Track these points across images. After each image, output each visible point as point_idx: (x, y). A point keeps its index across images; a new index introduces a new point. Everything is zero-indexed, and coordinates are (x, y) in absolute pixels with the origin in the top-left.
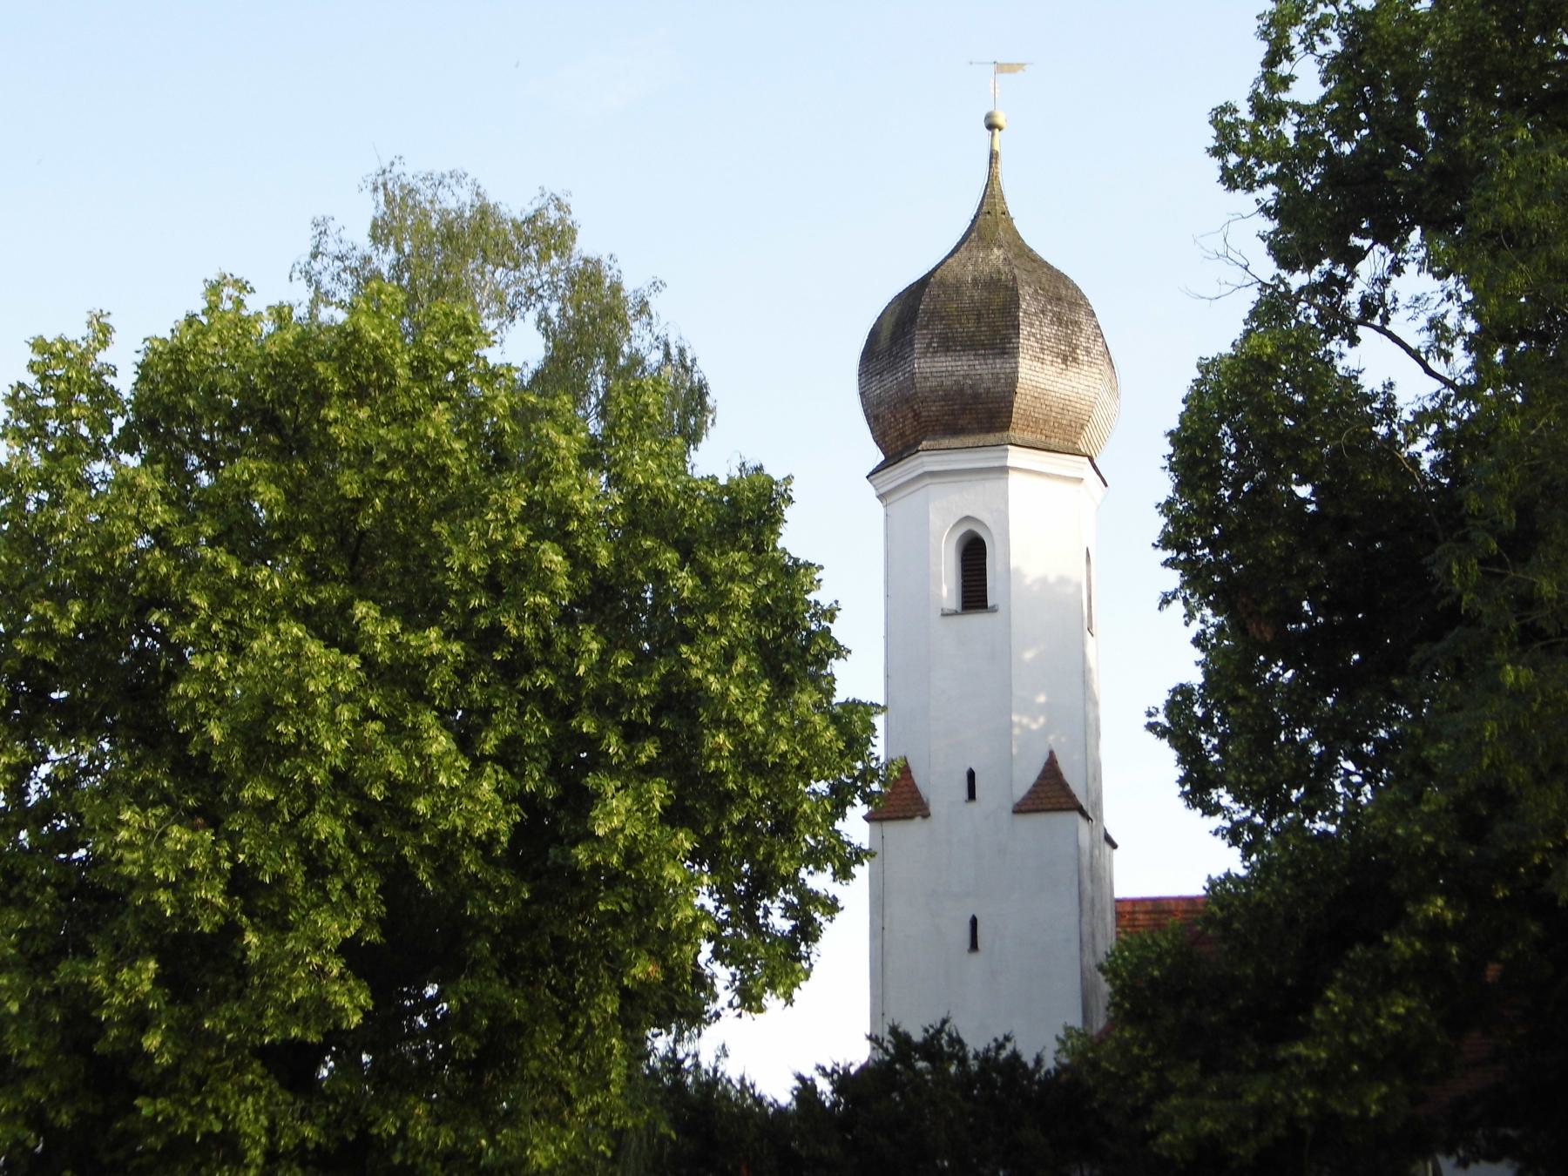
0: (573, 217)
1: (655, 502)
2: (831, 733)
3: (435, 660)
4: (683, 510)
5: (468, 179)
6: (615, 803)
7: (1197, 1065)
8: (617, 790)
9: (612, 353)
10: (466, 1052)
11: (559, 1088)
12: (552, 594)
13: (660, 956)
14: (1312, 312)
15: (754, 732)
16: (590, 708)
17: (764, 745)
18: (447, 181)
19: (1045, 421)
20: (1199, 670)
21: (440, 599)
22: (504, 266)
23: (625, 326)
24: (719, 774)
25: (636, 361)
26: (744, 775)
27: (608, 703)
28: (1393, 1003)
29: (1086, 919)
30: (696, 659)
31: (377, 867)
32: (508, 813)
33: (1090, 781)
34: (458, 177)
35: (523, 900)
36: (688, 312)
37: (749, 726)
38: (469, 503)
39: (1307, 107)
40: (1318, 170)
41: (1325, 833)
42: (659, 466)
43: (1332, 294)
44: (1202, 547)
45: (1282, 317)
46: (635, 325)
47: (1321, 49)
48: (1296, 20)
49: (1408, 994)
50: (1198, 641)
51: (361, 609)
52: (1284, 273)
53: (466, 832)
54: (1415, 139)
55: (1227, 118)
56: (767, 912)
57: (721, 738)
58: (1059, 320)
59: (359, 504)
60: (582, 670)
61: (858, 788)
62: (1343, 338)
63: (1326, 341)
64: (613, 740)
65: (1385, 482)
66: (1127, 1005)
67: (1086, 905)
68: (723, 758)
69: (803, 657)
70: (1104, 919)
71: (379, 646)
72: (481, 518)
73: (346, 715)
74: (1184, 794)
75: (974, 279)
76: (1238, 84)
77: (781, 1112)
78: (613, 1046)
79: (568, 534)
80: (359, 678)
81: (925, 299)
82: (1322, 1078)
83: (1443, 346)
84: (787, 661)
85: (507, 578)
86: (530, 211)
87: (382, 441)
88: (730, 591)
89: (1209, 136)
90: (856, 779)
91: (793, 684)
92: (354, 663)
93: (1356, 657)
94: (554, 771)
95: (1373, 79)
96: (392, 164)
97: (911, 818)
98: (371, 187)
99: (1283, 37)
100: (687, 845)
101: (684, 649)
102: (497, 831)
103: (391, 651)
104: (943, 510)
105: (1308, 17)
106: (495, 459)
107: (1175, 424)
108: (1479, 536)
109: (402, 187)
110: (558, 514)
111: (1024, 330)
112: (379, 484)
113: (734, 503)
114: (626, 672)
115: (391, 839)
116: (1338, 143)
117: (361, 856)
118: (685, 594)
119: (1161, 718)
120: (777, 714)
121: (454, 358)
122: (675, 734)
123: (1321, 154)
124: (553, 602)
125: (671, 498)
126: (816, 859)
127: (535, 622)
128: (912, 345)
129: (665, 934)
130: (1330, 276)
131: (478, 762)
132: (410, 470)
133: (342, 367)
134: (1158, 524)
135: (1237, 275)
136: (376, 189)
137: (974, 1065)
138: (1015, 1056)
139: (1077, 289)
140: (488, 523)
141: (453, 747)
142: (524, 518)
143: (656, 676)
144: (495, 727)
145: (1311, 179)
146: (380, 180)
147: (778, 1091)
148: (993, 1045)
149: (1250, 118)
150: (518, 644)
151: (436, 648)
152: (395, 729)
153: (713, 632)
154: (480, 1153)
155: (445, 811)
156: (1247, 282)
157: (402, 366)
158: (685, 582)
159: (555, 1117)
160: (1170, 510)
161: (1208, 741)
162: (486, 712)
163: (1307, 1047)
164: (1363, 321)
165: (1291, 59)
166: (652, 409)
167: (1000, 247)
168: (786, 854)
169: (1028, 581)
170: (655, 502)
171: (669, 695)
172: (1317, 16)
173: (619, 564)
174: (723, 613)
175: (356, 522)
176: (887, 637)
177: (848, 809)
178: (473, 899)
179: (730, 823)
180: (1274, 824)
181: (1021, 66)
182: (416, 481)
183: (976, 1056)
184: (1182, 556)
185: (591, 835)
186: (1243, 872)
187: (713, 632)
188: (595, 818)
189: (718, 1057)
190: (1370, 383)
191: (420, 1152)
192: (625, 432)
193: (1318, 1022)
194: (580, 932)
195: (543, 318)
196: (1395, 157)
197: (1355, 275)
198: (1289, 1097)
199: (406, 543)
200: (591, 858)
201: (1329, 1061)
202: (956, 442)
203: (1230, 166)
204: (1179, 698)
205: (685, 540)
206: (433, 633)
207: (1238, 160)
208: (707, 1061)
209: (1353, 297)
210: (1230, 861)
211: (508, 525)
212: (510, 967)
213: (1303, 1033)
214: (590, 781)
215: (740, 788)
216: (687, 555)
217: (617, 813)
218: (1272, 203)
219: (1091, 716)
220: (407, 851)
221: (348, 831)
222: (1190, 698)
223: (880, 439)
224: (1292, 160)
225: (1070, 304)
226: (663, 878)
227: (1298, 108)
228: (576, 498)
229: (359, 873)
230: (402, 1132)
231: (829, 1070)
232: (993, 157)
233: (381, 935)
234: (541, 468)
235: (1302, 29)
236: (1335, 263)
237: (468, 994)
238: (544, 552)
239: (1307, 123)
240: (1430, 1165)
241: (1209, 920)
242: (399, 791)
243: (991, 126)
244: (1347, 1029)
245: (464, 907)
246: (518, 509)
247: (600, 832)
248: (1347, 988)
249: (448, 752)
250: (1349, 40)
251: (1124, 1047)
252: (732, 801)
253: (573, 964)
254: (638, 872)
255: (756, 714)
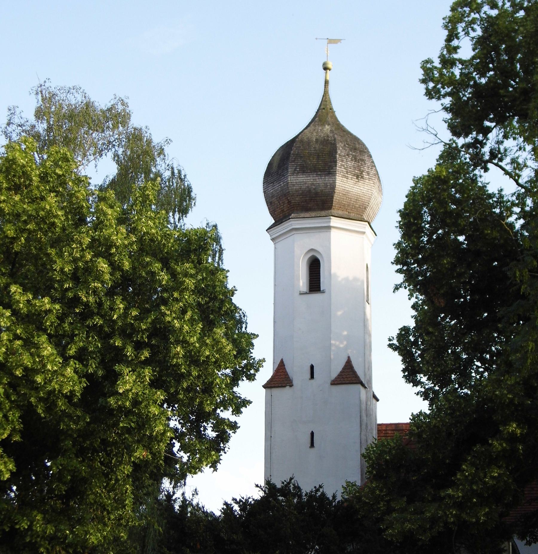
0: (129, 109)
1: (152, 240)
2: (230, 347)
3: (50, 311)
4: (164, 244)
5: (81, 90)
6: (128, 378)
7: (405, 499)
8: (130, 372)
9: (148, 172)
10: (61, 491)
11: (104, 508)
12: (103, 282)
13: (148, 448)
14: (468, 156)
15: (195, 346)
16: (120, 335)
17: (199, 352)
18: (72, 91)
19: (349, 205)
20: (413, 320)
21: (51, 284)
22: (97, 131)
23: (154, 160)
24: (178, 365)
25: (158, 174)
26: (189, 366)
27: (128, 332)
28: (492, 472)
29: (363, 433)
30: (168, 312)
31: (18, 407)
32: (80, 383)
33: (367, 370)
34: (76, 89)
35: (87, 422)
36: (182, 154)
37: (192, 344)
38: (61, 241)
39: (465, 61)
40: (470, 90)
41: (466, 394)
42: (154, 224)
43: (477, 148)
44: (413, 264)
45: (454, 158)
46: (158, 159)
47: (472, 34)
48: (461, 20)
49: (499, 467)
50: (414, 307)
51: (13, 288)
52: (455, 138)
53: (60, 391)
54: (514, 75)
55: (429, 66)
56: (205, 429)
57: (179, 349)
58: (355, 159)
59: (14, 240)
60: (115, 317)
61: (244, 372)
62: (482, 168)
63: (474, 170)
64: (130, 349)
65: (496, 234)
66: (375, 472)
67: (364, 427)
68: (180, 358)
69: (219, 312)
70: (372, 433)
71: (21, 305)
72: (70, 247)
73: (5, 337)
74: (404, 376)
75: (317, 140)
76: (433, 49)
77: (216, 519)
78: (127, 488)
79: (111, 254)
80: (12, 320)
81: (294, 149)
82: (460, 505)
83: (517, 171)
84: (212, 314)
85: (82, 275)
86: (109, 105)
87: (24, 211)
88: (185, 281)
89: (420, 74)
90: (243, 368)
91: (214, 324)
92: (8, 313)
93: (486, 314)
94: (102, 363)
95: (496, 49)
96: (45, 82)
97: (285, 387)
98: (35, 93)
99: (455, 28)
100: (162, 397)
101: (163, 308)
102: (74, 391)
103: (27, 308)
104: (301, 246)
105: (466, 19)
106: (79, 219)
107: (402, 207)
108: (529, 259)
109: (49, 93)
110: (107, 245)
111: (339, 163)
112: (23, 231)
113: (189, 241)
114: (136, 318)
115: (25, 394)
116: (480, 78)
117: (11, 402)
118: (164, 283)
119: (395, 342)
120: (206, 338)
121: (60, 173)
122: (158, 347)
123: (472, 83)
124: (103, 286)
125: (159, 238)
126: (224, 404)
127: (95, 295)
128: (287, 169)
129: (151, 437)
130: (476, 141)
131: (66, 359)
132: (37, 224)
133: (7, 176)
134: (394, 253)
135: (431, 139)
136: (37, 94)
137: (305, 499)
138: (323, 494)
139: (364, 145)
140: (73, 249)
141: (55, 352)
142: (90, 246)
143: (149, 320)
144: (75, 343)
145: (467, 94)
146: (39, 89)
147: (215, 508)
148: (314, 489)
149: (439, 66)
150: (87, 305)
151: (48, 306)
152: (28, 344)
153: (177, 300)
154: (66, 537)
155: (50, 381)
156: (436, 142)
157: (35, 176)
158: (164, 277)
159: (101, 520)
160: (399, 247)
161: (416, 352)
162: (72, 336)
163: (453, 491)
164: (490, 161)
165: (458, 38)
166: (151, 197)
167: (329, 125)
168: (208, 402)
169: (340, 279)
170: (152, 240)
171: (155, 328)
172: (470, 19)
173: (134, 268)
174: (181, 292)
175: (13, 248)
176: (274, 304)
177: (240, 382)
178: (64, 422)
179: (183, 388)
180: (444, 390)
181: (339, 40)
182: (41, 229)
183: (306, 495)
184: (405, 268)
185: (117, 393)
186: (428, 412)
187: (177, 300)
188: (118, 385)
189: (193, 495)
190: (492, 189)
191: (38, 536)
192: (138, 208)
193: (459, 480)
194: (113, 437)
195: (116, 155)
196: (507, 85)
197: (488, 139)
198: (445, 513)
199: (37, 258)
200: (116, 403)
201: (463, 497)
202: (307, 215)
203: (430, 88)
204: (403, 333)
205: (166, 258)
206: (46, 300)
207: (434, 85)
208: (188, 496)
209: (486, 150)
210: (424, 406)
211: (83, 250)
212: (81, 452)
213: (453, 485)
214: (117, 368)
215: (188, 371)
216: (165, 263)
217: (129, 383)
218: (449, 105)
219: (368, 341)
220: (32, 400)
221: (5, 390)
222: (408, 333)
223: (273, 213)
224: (457, 86)
225: (361, 151)
226: (150, 412)
227: (461, 62)
228: (115, 238)
229: (10, 409)
230: (30, 527)
231: (238, 500)
232: (326, 83)
233: (21, 438)
234: (99, 224)
235: (463, 25)
236: (478, 134)
237: (61, 465)
238: (99, 263)
239: (465, 68)
240: (511, 543)
241: (411, 433)
242: (29, 372)
243: (326, 68)
244: (472, 483)
245: (60, 425)
246: (87, 243)
247: (121, 391)
248: (473, 464)
249: (52, 354)
250: (485, 30)
251: (372, 491)
252: (184, 377)
253: (111, 451)
254: (139, 409)
255: (195, 338)
